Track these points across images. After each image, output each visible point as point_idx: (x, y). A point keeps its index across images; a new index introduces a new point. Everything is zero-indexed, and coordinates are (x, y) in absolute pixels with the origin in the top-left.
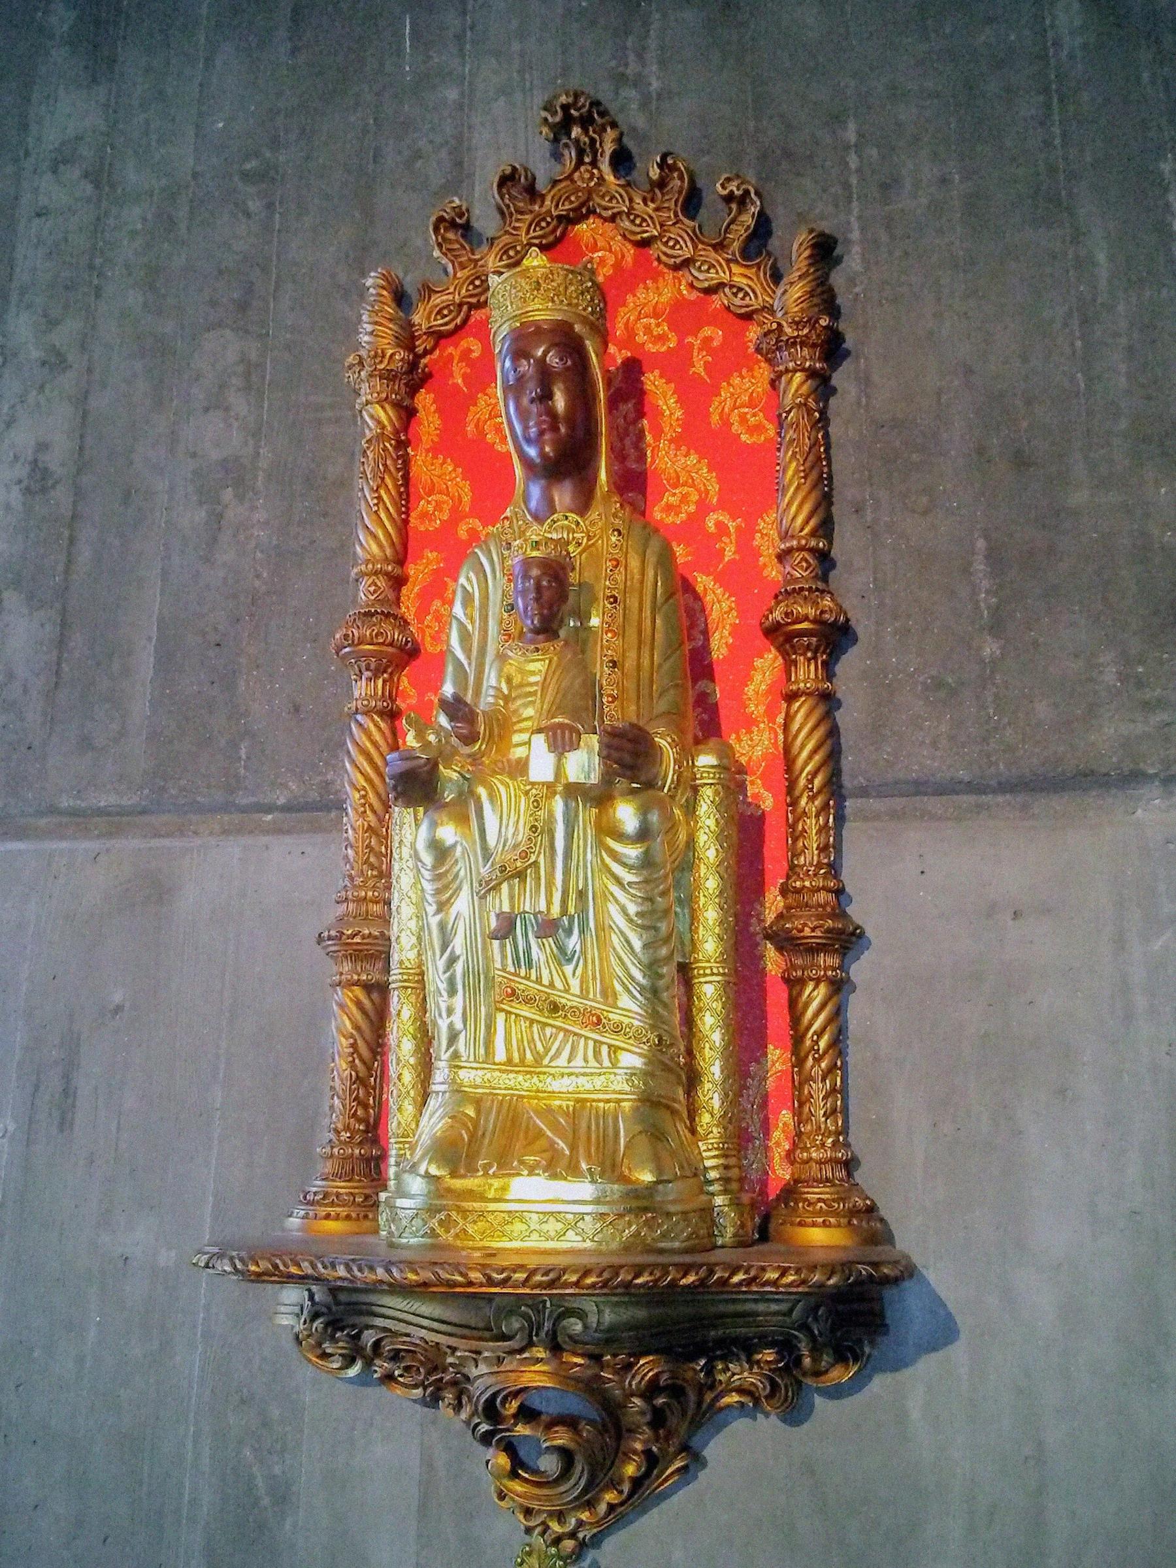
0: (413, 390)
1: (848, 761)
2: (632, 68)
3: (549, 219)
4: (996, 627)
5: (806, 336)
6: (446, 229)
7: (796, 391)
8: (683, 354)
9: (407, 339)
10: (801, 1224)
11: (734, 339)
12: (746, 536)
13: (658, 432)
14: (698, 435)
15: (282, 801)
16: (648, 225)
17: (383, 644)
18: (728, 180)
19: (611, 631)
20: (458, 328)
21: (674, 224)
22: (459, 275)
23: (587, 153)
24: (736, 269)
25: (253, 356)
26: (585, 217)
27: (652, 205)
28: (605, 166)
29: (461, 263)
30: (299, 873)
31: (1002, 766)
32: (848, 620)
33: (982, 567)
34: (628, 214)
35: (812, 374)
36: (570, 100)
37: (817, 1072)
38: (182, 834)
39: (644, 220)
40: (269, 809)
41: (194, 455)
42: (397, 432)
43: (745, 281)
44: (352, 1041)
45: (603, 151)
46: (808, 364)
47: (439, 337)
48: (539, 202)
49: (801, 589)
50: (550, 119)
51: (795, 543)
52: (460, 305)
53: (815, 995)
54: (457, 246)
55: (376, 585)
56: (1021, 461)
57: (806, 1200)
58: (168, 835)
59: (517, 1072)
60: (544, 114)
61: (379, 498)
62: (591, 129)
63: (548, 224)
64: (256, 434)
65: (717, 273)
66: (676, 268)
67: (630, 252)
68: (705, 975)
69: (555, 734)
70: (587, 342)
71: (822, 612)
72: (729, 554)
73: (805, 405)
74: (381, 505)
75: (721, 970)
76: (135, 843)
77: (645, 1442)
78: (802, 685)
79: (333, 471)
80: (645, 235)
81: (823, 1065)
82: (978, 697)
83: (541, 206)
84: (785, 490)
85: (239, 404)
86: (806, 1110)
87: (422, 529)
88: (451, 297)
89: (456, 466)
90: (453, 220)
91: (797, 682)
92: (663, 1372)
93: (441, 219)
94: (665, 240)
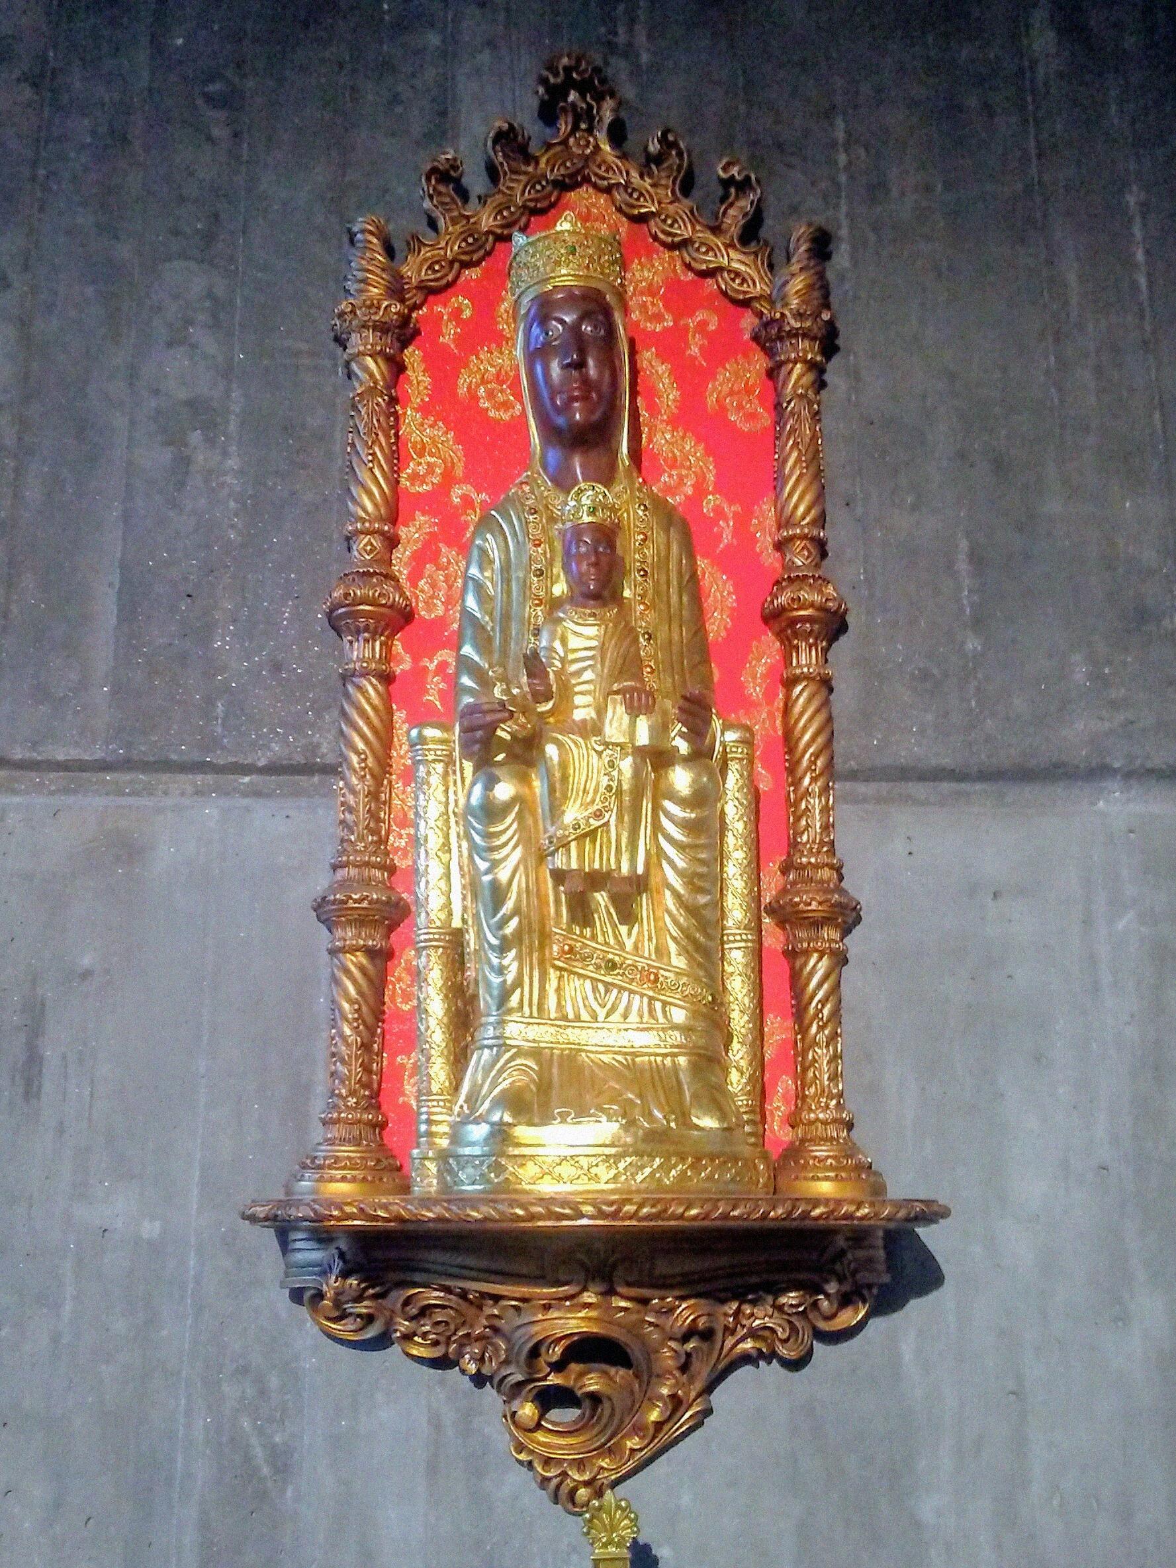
0: (405, 343)
1: (839, 745)
2: (622, 38)
3: (544, 183)
4: (978, 623)
6: (438, 181)
7: (796, 382)
8: (678, 335)
9: (396, 290)
10: (806, 1179)
11: (730, 327)
12: (742, 522)
13: (653, 409)
14: (692, 416)
15: (262, 763)
16: (646, 200)
19: (644, 603)
20: (450, 285)
22: (450, 229)
23: (585, 119)
24: (732, 254)
25: (220, 291)
27: (648, 181)
29: (452, 219)
30: (294, 839)
31: (983, 756)
32: (846, 610)
34: (626, 187)
35: (812, 366)
36: (573, 63)
37: (821, 1038)
39: (641, 194)
41: (156, 392)
42: (388, 387)
43: (743, 268)
44: (356, 1007)
45: (601, 120)
46: (809, 357)
48: (533, 165)
50: (552, 80)
51: (798, 531)
52: (452, 263)
53: (816, 967)
54: (447, 200)
55: (372, 544)
56: (1000, 466)
59: (574, 1027)
60: (545, 73)
61: (374, 454)
63: (543, 187)
66: (672, 247)
67: (624, 227)
68: (735, 941)
69: (632, 697)
72: (727, 538)
75: (750, 937)
76: (99, 801)
77: (671, 1387)
78: (805, 670)
79: (315, 421)
80: (643, 211)
81: (826, 1032)
83: (536, 168)
85: (209, 344)
86: (810, 1074)
88: (442, 252)
89: (448, 429)
91: (799, 665)
92: (699, 1316)
93: (434, 170)
94: (663, 217)
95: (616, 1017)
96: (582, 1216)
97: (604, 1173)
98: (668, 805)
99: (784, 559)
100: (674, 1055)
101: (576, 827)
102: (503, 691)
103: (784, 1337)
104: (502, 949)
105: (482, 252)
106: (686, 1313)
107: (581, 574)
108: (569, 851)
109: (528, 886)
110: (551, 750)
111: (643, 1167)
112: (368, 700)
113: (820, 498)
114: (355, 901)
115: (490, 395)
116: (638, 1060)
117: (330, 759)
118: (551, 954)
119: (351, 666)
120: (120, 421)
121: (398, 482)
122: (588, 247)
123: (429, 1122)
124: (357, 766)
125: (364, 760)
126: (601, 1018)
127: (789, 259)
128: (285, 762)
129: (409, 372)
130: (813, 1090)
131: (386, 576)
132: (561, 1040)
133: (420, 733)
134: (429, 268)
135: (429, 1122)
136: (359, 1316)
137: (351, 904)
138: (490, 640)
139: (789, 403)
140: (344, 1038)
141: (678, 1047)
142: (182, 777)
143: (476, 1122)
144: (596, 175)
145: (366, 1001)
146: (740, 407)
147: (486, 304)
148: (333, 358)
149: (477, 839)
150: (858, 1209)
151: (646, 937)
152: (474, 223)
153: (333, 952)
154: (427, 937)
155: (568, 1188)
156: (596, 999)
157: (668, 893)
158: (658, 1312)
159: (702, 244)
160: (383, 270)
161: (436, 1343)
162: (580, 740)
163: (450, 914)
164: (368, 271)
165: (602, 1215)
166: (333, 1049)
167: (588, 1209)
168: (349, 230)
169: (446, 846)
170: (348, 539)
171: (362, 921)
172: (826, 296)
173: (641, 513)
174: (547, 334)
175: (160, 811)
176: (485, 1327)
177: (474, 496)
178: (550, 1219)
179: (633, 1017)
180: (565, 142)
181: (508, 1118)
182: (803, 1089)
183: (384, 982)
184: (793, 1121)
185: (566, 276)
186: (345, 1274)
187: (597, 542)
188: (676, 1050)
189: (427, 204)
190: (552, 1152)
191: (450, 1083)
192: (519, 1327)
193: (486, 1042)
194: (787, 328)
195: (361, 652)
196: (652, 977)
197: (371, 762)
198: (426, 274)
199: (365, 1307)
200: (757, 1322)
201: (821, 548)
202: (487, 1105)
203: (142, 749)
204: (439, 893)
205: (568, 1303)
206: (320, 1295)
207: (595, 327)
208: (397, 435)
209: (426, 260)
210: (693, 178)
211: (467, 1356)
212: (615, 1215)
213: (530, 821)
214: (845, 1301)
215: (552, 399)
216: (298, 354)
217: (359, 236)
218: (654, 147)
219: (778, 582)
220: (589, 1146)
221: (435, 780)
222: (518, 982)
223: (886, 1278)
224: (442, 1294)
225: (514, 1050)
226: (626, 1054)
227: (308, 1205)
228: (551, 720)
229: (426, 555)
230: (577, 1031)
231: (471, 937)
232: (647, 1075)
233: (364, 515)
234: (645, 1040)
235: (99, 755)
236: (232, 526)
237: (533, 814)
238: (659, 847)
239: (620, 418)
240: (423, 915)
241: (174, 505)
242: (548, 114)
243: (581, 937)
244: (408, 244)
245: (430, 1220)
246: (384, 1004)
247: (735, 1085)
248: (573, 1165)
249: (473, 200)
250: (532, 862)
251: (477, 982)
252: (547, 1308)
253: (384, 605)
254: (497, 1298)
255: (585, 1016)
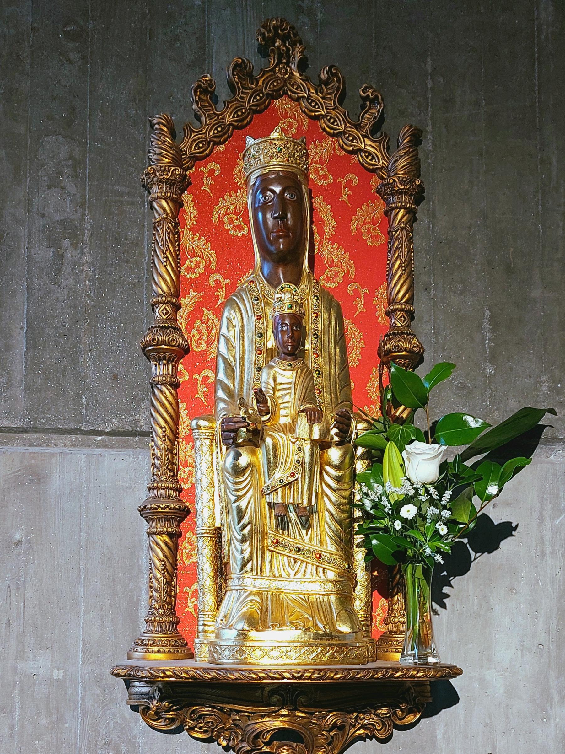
4: (493, 359)
5: (408, 189)
9: (177, 161)
11: (364, 185)
12: (369, 298)
13: (322, 234)
14: (342, 238)
16: (319, 108)
17: (174, 346)
18: (366, 88)
19: (316, 354)
20: (208, 155)
21: (333, 109)
23: (284, 57)
24: (368, 142)
25: (77, 153)
26: (281, 96)
28: (294, 67)
29: (209, 115)
30: (128, 473)
33: (488, 326)
35: (409, 211)
38: (47, 446)
39: (317, 104)
40: (100, 433)
41: (43, 216)
42: (174, 217)
43: (373, 150)
45: (294, 57)
46: (408, 205)
47: (195, 159)
49: (402, 333)
51: (399, 306)
52: (209, 142)
55: (166, 310)
56: (509, 270)
57: (397, 641)
58: (40, 445)
61: (167, 257)
62: (287, 42)
64: (82, 205)
65: (357, 143)
66: (333, 135)
69: (310, 414)
70: (303, 186)
71: (414, 347)
73: (405, 228)
74: (168, 262)
79: (133, 234)
80: (317, 113)
82: (482, 395)
84: (394, 276)
87: (188, 276)
90: (207, 88)
93: (199, 86)
95: (300, 575)
96: (284, 678)
97: (292, 654)
98: (327, 468)
99: (391, 322)
100: (328, 595)
101: (281, 481)
102: (245, 412)
103: (379, 728)
104: (243, 541)
105: (226, 136)
106: (331, 718)
107: (284, 342)
108: (277, 493)
109: (255, 508)
110: (269, 441)
111: (312, 652)
112: (166, 398)
113: (411, 288)
114: (162, 508)
115: (231, 221)
116: (310, 597)
117: (145, 428)
118: (267, 543)
119: (157, 379)
120: (23, 232)
121: (180, 272)
122: (288, 148)
123: (204, 625)
124: (161, 435)
125: (165, 432)
126: (292, 576)
127: (398, 146)
128: (120, 430)
129: (185, 207)
130: (397, 606)
131: (175, 329)
132: (272, 587)
133: (197, 424)
134: (196, 146)
135: (204, 625)
136: (167, 718)
137: (159, 510)
138: (233, 371)
139: (396, 232)
140: (157, 579)
141: (331, 591)
142: (63, 436)
143: (229, 628)
144: (290, 90)
145: (168, 560)
146: (369, 232)
147: (229, 165)
148: (142, 196)
149: (230, 485)
150: (418, 673)
151: (315, 535)
152: (221, 119)
153: (149, 534)
154: (202, 531)
155: (276, 662)
156: (289, 566)
157: (327, 513)
158: (318, 718)
159: (350, 135)
160: (171, 148)
161: (205, 731)
162: (283, 435)
163: (214, 519)
164: (162, 148)
165: (294, 677)
166: (151, 585)
167: (287, 675)
168: (151, 121)
169: (212, 484)
170: (153, 306)
171: (165, 519)
172: (418, 169)
173: (315, 301)
174: (265, 198)
175: (54, 455)
176: (232, 724)
177: (222, 281)
178: (269, 679)
179: (308, 575)
180: (273, 70)
181: (246, 627)
182: (392, 606)
183: (176, 549)
184: (386, 621)
185: (276, 164)
186: (161, 700)
187: (292, 325)
188: (329, 592)
189: (194, 106)
190: (267, 645)
191: (215, 606)
192: (249, 725)
193: (233, 588)
194: (397, 189)
195: (160, 370)
196: (318, 556)
197: (168, 432)
198: (195, 149)
199: (172, 715)
200: (366, 721)
201: (411, 315)
202: (235, 620)
203: (42, 422)
204: (208, 510)
205: (274, 714)
206: (149, 708)
207: (292, 196)
208: (179, 245)
209: (195, 140)
210: (345, 94)
211: (222, 738)
212: (300, 678)
213: (257, 476)
214: (410, 711)
215: (268, 236)
216: (121, 194)
217: (157, 126)
218: (324, 76)
219: (387, 335)
220: (287, 641)
221: (205, 448)
222: (250, 559)
223: (431, 700)
224: (210, 709)
225: (248, 592)
226: (304, 594)
227: (148, 670)
228: (269, 424)
229: (196, 314)
230: (280, 583)
231: (225, 533)
232: (315, 605)
233: (162, 293)
234: (314, 587)
235: (19, 424)
236: (88, 296)
237: (259, 472)
238: (322, 489)
239: (304, 246)
240: (200, 520)
241: (56, 282)
242: (264, 50)
243: (284, 538)
244: (184, 129)
245: (209, 679)
246: (177, 560)
247: (358, 607)
248: (279, 652)
249: (221, 105)
250: (258, 497)
251: (229, 556)
252: (263, 716)
253: (174, 346)
254: (238, 712)
255: (284, 575)
